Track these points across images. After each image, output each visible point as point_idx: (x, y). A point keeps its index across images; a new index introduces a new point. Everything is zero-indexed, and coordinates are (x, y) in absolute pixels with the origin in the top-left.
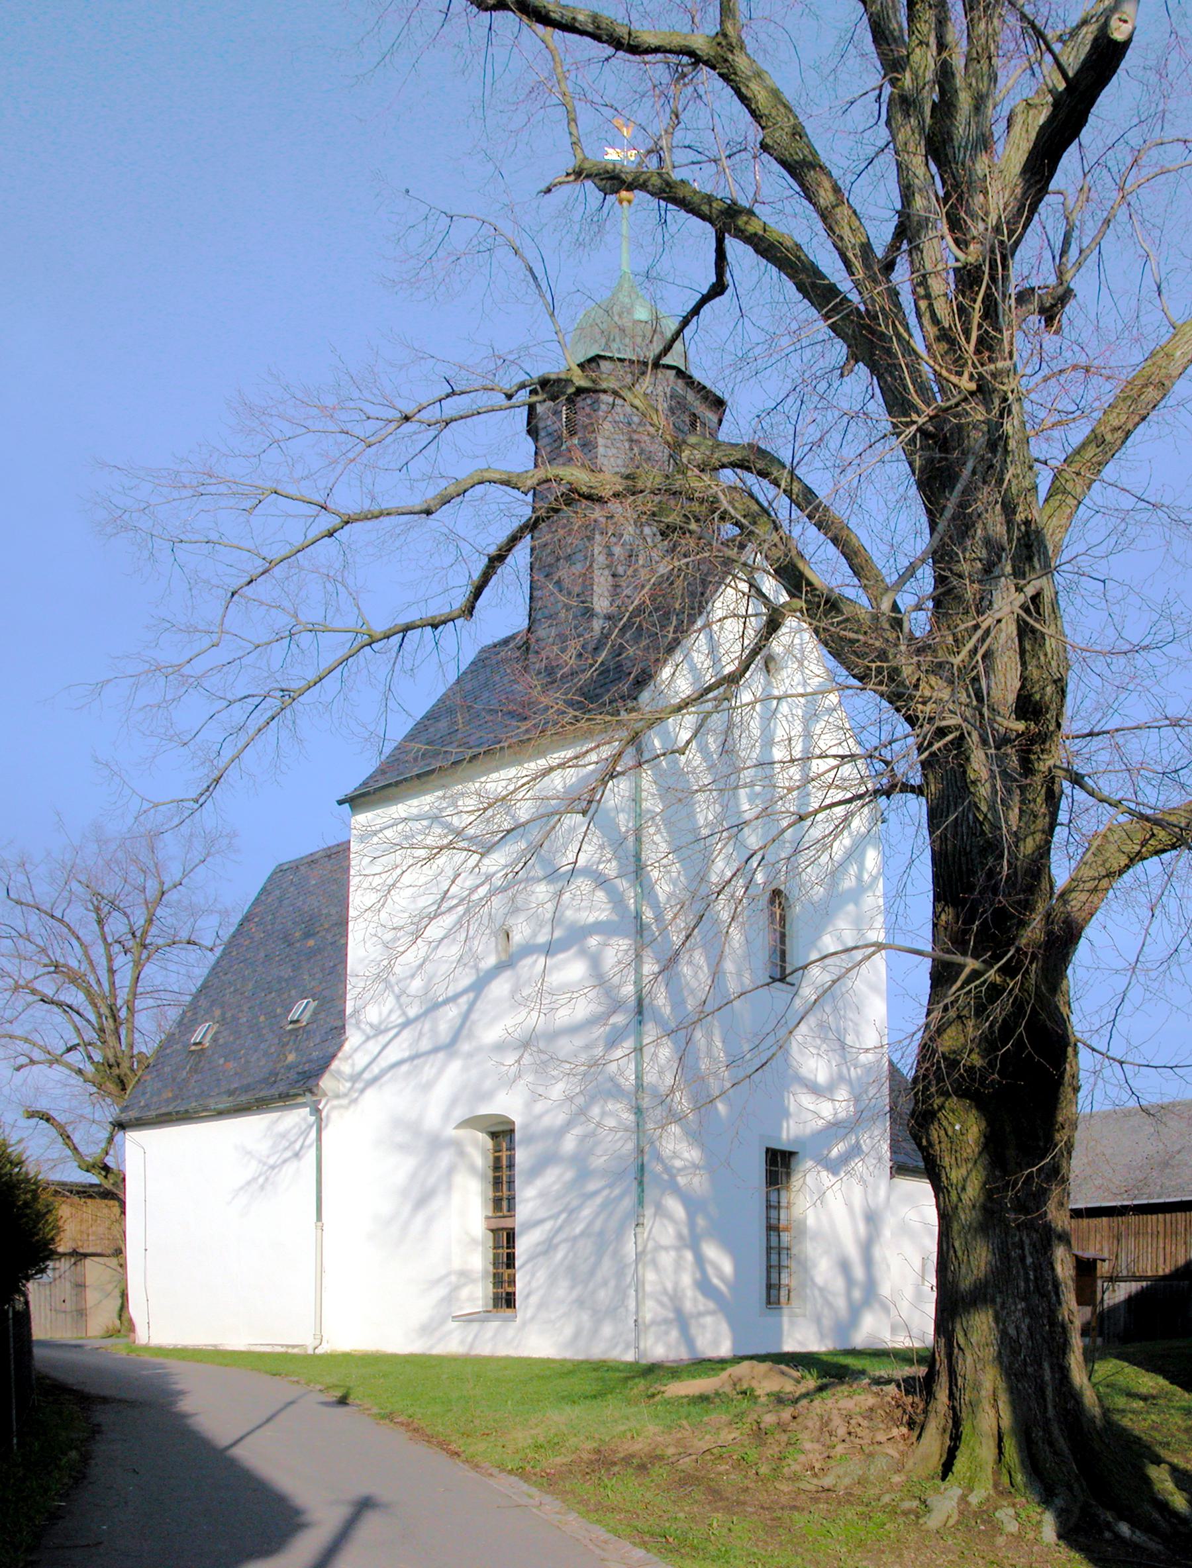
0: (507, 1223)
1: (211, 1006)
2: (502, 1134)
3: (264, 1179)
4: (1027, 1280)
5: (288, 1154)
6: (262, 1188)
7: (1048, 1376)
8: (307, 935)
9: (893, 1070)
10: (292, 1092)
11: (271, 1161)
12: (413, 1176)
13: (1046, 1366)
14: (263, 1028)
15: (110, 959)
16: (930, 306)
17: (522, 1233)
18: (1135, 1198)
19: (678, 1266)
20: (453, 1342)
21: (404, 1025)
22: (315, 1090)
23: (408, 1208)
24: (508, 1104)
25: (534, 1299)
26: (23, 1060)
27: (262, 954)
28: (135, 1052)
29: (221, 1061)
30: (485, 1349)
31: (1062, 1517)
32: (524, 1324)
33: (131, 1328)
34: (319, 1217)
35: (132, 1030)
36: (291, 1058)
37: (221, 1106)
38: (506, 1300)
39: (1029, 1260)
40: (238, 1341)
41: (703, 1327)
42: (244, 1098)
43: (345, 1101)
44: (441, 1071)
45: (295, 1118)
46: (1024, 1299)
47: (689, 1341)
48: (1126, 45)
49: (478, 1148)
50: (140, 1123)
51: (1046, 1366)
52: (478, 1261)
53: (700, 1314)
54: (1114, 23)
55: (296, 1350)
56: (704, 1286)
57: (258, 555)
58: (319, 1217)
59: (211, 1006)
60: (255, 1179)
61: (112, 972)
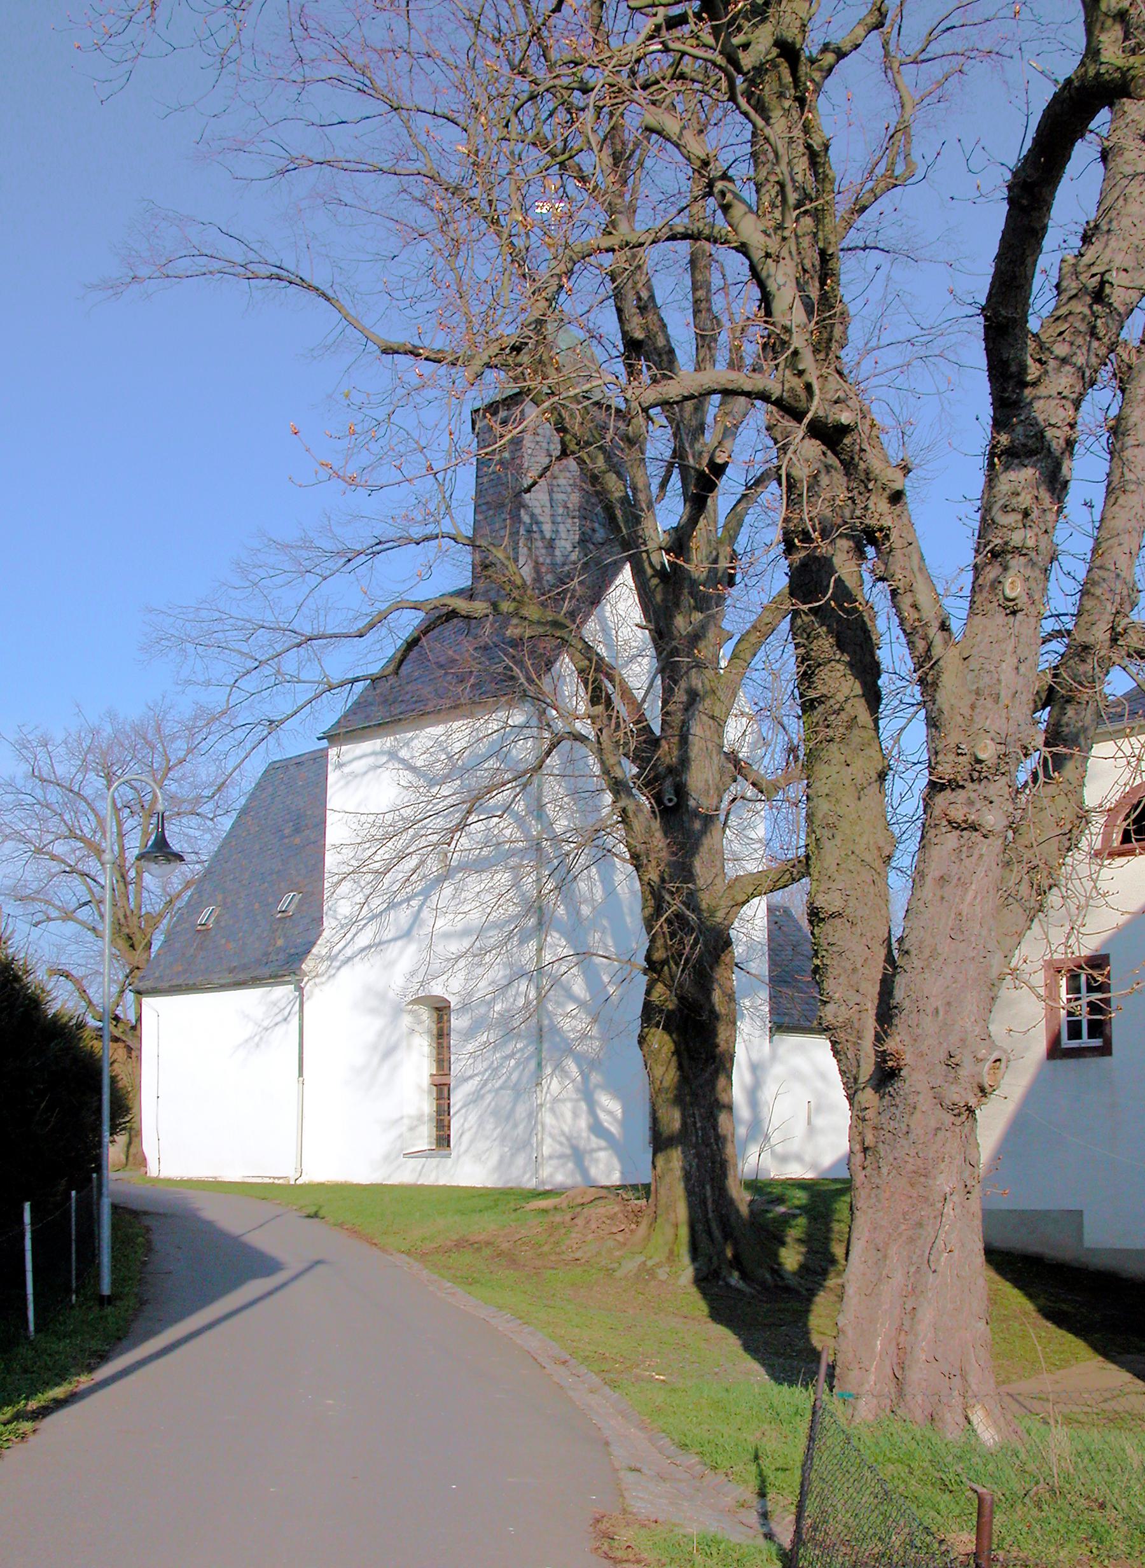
0: (444, 1080)
1: (214, 891)
2: (441, 1010)
3: (258, 1039)
4: (697, 1137)
5: (279, 1018)
6: (257, 1045)
7: (709, 1193)
8: (297, 830)
9: (419, 1087)
10: (281, 973)
11: (265, 1024)
12: (381, 1034)
13: (708, 1187)
14: (257, 926)
15: (120, 824)
16: (648, 557)
17: (456, 1087)
18: (823, 1076)
19: (575, 1115)
20: (406, 1174)
21: (371, 919)
22: (298, 972)
23: (376, 1060)
24: (449, 988)
25: (466, 1138)
26: (40, 917)
27: (257, 847)
28: (143, 911)
29: (223, 941)
30: (429, 1180)
31: (697, 1270)
32: (459, 1157)
33: (143, 1161)
34: (301, 1074)
35: (139, 894)
36: (280, 942)
37: (222, 981)
38: (443, 1140)
39: (699, 1125)
40: (233, 1173)
41: (597, 1161)
42: (242, 976)
43: (324, 979)
44: (401, 952)
45: (282, 993)
46: (695, 1148)
47: (584, 1172)
48: (726, 464)
49: (426, 1015)
50: (154, 992)
51: (708, 1187)
52: (427, 1106)
53: (593, 1150)
54: (717, 453)
55: (281, 1181)
56: (597, 1128)
57: (252, 657)
58: (301, 1074)
59: (214, 891)
60: (251, 1038)
61: (121, 835)
